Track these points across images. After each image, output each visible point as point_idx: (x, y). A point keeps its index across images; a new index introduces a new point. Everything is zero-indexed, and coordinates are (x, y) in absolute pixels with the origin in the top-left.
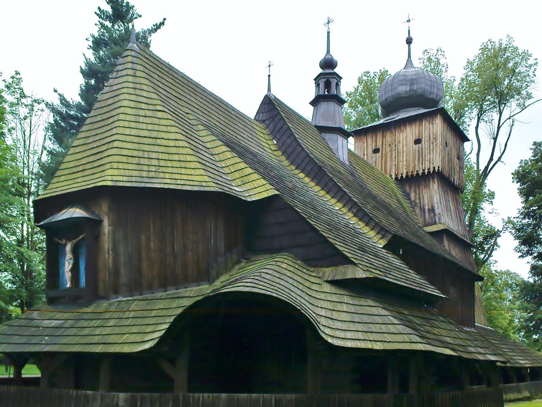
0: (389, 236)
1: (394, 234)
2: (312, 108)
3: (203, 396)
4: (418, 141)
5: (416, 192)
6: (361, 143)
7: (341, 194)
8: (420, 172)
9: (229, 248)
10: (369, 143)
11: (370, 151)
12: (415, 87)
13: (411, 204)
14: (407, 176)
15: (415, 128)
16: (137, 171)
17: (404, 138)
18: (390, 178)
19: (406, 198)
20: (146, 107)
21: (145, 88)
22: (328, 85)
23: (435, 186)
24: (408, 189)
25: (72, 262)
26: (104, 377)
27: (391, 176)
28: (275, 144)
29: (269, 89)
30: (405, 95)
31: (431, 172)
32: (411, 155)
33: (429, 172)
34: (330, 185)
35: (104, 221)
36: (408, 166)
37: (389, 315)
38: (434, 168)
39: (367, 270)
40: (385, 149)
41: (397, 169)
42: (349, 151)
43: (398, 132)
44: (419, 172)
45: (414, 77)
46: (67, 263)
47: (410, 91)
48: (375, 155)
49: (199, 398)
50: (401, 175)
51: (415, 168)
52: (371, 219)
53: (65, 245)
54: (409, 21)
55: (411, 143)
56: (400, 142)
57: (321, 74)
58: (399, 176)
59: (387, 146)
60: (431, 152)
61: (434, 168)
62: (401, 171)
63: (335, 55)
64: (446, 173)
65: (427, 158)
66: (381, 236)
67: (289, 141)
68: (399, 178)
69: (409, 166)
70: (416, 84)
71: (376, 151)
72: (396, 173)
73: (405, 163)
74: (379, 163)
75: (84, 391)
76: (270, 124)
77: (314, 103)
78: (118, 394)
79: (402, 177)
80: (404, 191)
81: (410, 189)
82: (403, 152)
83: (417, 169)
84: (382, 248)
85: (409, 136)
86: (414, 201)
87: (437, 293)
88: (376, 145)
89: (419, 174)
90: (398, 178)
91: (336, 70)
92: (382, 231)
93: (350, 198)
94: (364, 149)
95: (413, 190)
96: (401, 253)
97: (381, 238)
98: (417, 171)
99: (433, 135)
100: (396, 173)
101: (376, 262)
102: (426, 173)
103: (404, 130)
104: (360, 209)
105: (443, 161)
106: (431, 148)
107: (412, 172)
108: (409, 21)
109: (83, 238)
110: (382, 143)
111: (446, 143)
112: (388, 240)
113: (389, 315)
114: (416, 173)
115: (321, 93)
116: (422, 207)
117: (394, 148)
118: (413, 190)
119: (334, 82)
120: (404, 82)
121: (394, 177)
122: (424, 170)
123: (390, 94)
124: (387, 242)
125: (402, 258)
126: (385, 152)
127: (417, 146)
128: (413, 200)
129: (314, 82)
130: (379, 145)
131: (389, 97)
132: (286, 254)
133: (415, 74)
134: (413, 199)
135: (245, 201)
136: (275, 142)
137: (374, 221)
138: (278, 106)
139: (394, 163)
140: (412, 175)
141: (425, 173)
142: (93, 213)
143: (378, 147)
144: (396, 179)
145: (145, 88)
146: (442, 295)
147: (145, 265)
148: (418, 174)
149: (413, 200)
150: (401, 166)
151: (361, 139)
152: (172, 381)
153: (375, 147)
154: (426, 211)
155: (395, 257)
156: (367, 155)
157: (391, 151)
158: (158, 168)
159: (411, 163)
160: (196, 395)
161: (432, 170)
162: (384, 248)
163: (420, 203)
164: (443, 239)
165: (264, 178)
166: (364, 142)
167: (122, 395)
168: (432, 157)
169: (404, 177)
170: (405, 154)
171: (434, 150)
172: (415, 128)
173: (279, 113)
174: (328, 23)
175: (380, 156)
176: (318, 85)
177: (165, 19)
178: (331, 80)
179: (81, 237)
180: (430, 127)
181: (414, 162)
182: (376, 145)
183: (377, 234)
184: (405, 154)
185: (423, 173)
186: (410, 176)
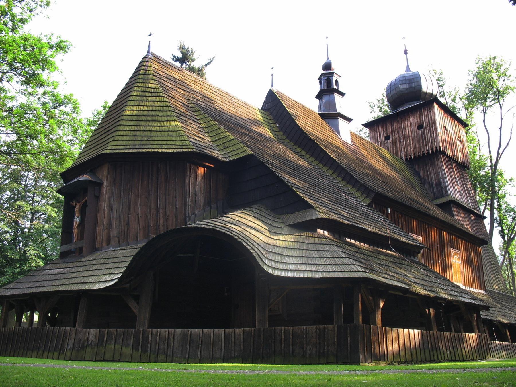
0: (373, 195)
2: (318, 101)
4: (420, 127)
5: (424, 170)
9: (208, 203)
11: (382, 138)
12: (413, 85)
13: (421, 180)
14: (415, 157)
15: (417, 116)
16: (132, 141)
17: (409, 125)
18: (401, 159)
28: (277, 127)
30: (406, 92)
31: (434, 151)
32: (416, 138)
33: (432, 152)
36: (414, 148)
37: (339, 251)
40: (395, 136)
41: (406, 152)
43: (403, 121)
44: (424, 153)
45: (412, 77)
47: (409, 88)
48: (386, 141)
49: (157, 334)
50: (409, 157)
51: (420, 150)
55: (415, 129)
56: (406, 129)
57: (322, 74)
59: (396, 133)
61: (436, 148)
65: (430, 140)
66: (366, 196)
68: (409, 159)
69: (416, 148)
70: (414, 82)
72: (405, 154)
73: (412, 145)
74: (390, 148)
76: (273, 111)
77: (319, 96)
79: (411, 158)
80: (414, 170)
82: (409, 137)
84: (366, 206)
85: (412, 124)
86: (423, 178)
88: (387, 133)
89: (424, 154)
90: (407, 159)
93: (339, 165)
94: (378, 137)
95: (421, 169)
97: (366, 197)
98: (423, 152)
100: (405, 154)
102: (430, 153)
103: (408, 118)
106: (432, 132)
107: (419, 153)
111: (445, 127)
112: (371, 199)
113: (339, 251)
114: (426, 152)
116: (430, 182)
117: (401, 134)
118: (421, 169)
120: (404, 82)
121: (404, 158)
122: (428, 150)
123: (394, 92)
124: (371, 200)
126: (395, 138)
127: (420, 131)
128: (422, 177)
129: (318, 81)
130: (389, 133)
131: (394, 94)
132: (258, 205)
133: (412, 75)
136: (278, 125)
138: (279, 96)
139: (403, 146)
140: (419, 155)
141: (429, 153)
143: (388, 135)
144: (406, 159)
148: (423, 154)
149: (422, 176)
150: (409, 148)
151: (374, 129)
153: (386, 135)
154: (434, 186)
156: (380, 141)
157: (399, 137)
158: (149, 137)
159: (417, 145)
166: (377, 132)
168: (433, 139)
170: (411, 138)
171: (434, 133)
172: (417, 116)
175: (391, 141)
176: (321, 83)
180: (428, 114)
181: (419, 144)
183: (362, 194)
184: (411, 138)
186: (417, 157)
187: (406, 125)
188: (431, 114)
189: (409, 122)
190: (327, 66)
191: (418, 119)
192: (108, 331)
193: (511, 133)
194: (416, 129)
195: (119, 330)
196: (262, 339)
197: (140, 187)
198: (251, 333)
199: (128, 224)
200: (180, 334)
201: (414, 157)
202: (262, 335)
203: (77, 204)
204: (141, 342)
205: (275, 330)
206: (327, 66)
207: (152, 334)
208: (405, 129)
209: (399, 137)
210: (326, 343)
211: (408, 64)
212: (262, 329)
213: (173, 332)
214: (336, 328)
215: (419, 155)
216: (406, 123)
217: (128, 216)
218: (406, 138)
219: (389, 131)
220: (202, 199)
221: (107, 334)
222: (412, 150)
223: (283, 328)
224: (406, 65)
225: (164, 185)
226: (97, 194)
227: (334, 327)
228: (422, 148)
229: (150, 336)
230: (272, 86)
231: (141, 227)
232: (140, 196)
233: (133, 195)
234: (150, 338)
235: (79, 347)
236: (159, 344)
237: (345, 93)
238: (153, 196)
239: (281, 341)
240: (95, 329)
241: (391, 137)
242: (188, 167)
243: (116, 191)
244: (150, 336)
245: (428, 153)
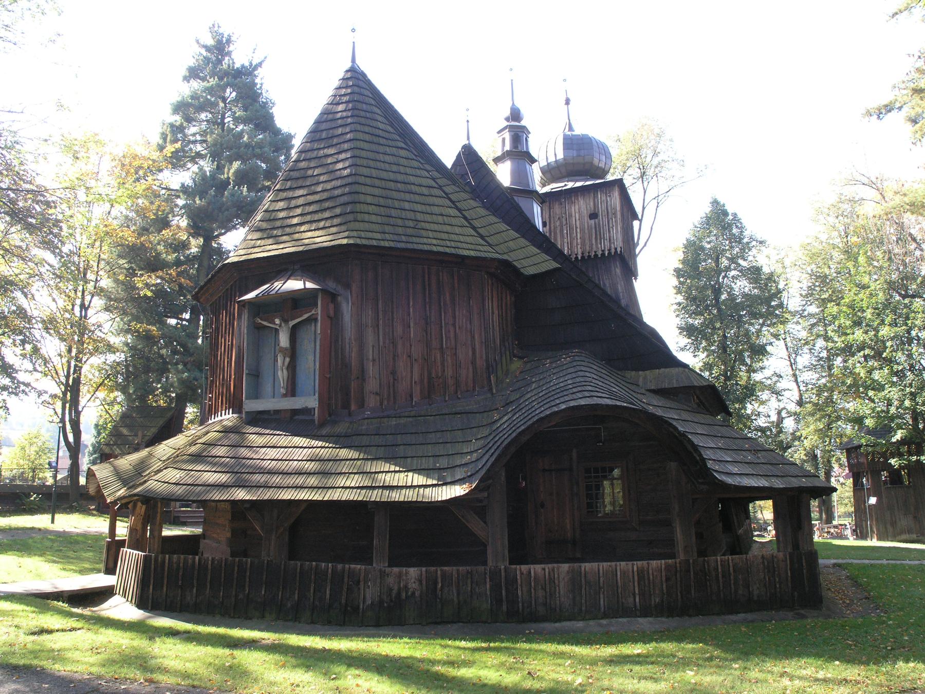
4: (593, 216)
8: (599, 253)
12: (582, 153)
14: (583, 257)
17: (577, 211)
33: (610, 253)
54: (468, 110)
60: (611, 229)
61: (616, 249)
63: (518, 105)
73: (579, 241)
75: (347, 566)
78: (648, 563)
82: (576, 228)
99: (612, 210)
106: (611, 225)
110: (550, 215)
114: (600, 252)
127: (592, 222)
140: (589, 256)
148: (596, 255)
157: (561, 226)
159: (587, 241)
161: (613, 251)
167: (413, 572)
169: (579, 258)
170: (578, 230)
177: (265, 58)
178: (520, 134)
184: (578, 230)
187: (573, 210)
188: (611, 201)
189: (577, 207)
190: (515, 115)
191: (592, 204)
192: (442, 570)
193: (652, 228)
194: (586, 218)
195: (461, 568)
198: (676, 567)
200: (568, 572)
201: (582, 257)
204: (504, 588)
206: (515, 115)
207: (522, 574)
208: (570, 216)
209: (561, 226)
210: (777, 579)
212: (691, 561)
215: (589, 256)
216: (573, 208)
218: (571, 228)
221: (442, 576)
222: (579, 247)
228: (594, 246)
230: (468, 139)
231: (416, 380)
235: (391, 601)
236: (535, 589)
237: (707, 209)
239: (717, 576)
240: (416, 569)
241: (548, 224)
243: (370, 312)
245: (603, 254)
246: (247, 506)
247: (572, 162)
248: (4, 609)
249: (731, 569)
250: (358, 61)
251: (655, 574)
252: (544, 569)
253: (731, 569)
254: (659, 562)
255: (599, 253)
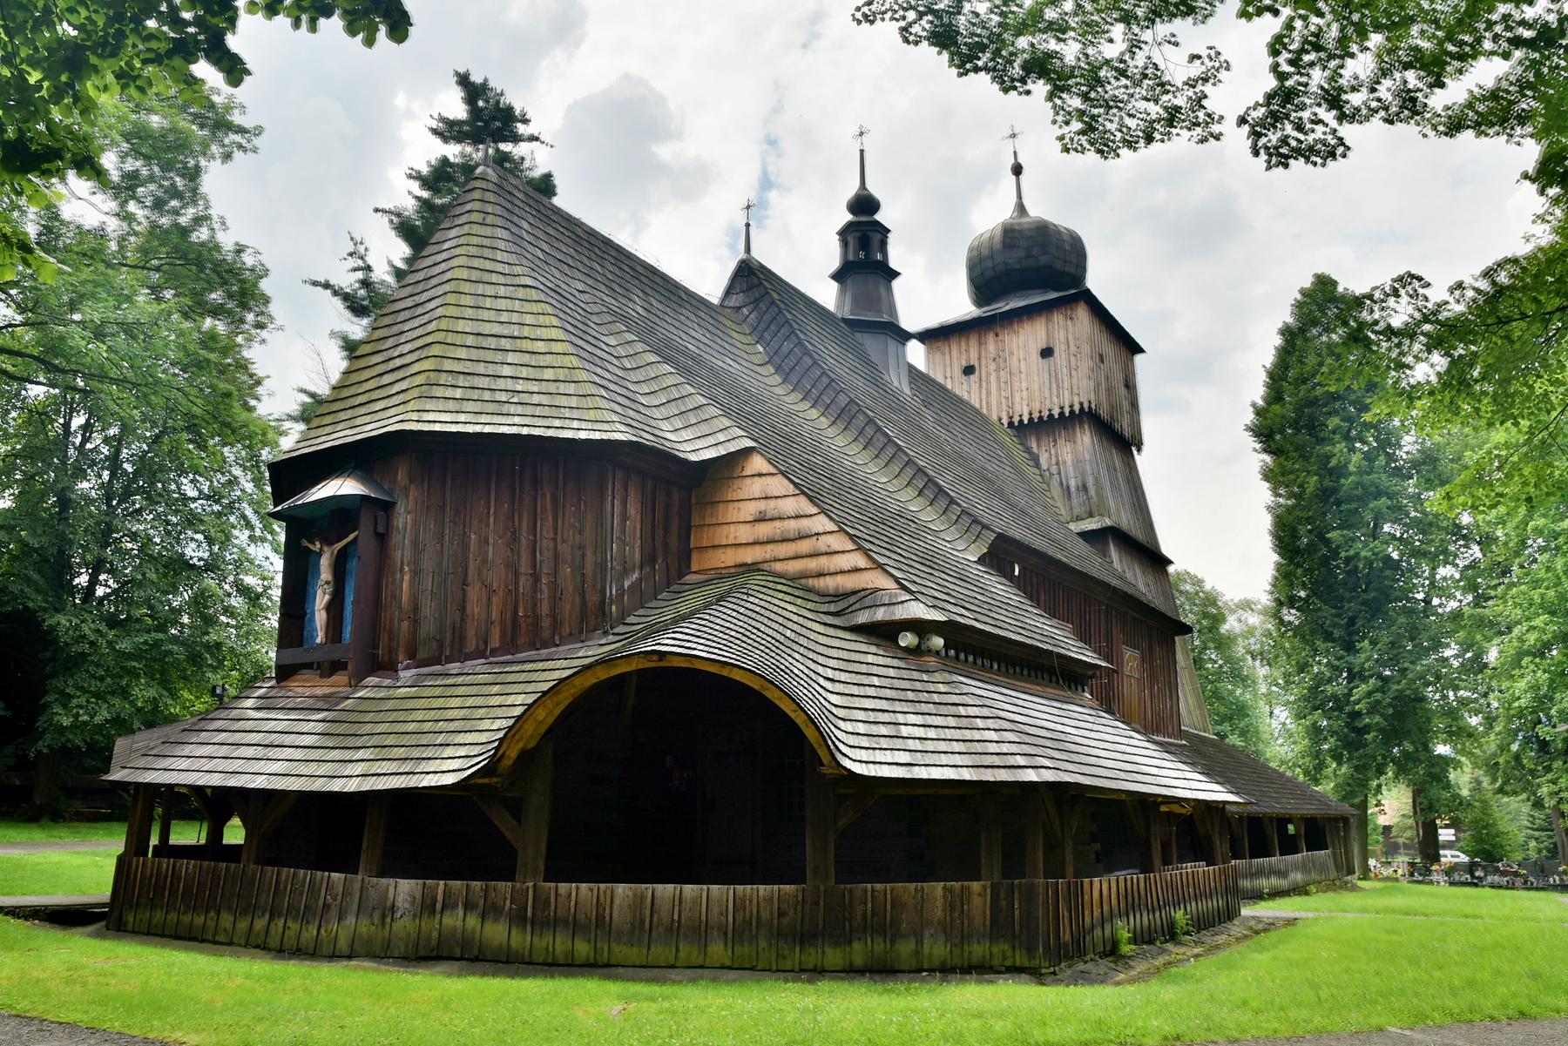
1: (999, 534)
2: (835, 285)
3: (578, 888)
4: (1047, 353)
6: (938, 356)
7: (890, 451)
8: (1056, 413)
10: (960, 353)
14: (1031, 419)
19: (1031, 463)
20: (502, 280)
21: (502, 245)
22: (864, 243)
23: (1085, 439)
24: (1034, 445)
25: (329, 589)
26: (370, 848)
27: (1000, 419)
29: (748, 249)
33: (1072, 412)
34: (869, 431)
35: (398, 506)
36: (1030, 400)
38: (1081, 404)
39: (934, 607)
42: (912, 370)
46: (319, 592)
49: (570, 895)
52: (952, 501)
53: (320, 555)
54: (1013, 136)
58: (1016, 420)
61: (1081, 404)
62: (1017, 409)
63: (874, 189)
64: (1104, 413)
67: (787, 346)
71: (969, 370)
80: (1028, 450)
81: (1039, 446)
83: (1048, 405)
87: (1089, 657)
88: (968, 359)
91: (878, 217)
92: (974, 524)
96: (1017, 573)
101: (960, 590)
104: (930, 480)
105: (1097, 391)
108: (1013, 136)
109: (355, 539)
115: (851, 258)
119: (876, 237)
121: (1005, 421)
122: (1062, 408)
125: (1022, 585)
134: (1044, 466)
135: (686, 461)
136: (761, 349)
137: (959, 505)
139: (1003, 394)
140: (1041, 418)
142: (385, 492)
144: (1011, 424)
145: (502, 245)
146: (1099, 663)
147: (474, 593)
148: (1051, 416)
152: (512, 853)
155: (1005, 581)
160: (563, 887)
162: (981, 561)
163: (1059, 473)
164: (1109, 549)
165: (727, 415)
173: (767, 293)
174: (861, 134)
178: (871, 234)
179: (352, 536)
182: (968, 359)
185: (1062, 414)
190: (864, 205)
196: (821, 912)
197: (492, 519)
199: (463, 609)
202: (822, 904)
203: (325, 548)
205: (851, 892)
206: (864, 205)
207: (557, 895)
211: (1019, 196)
213: (609, 892)
214: (988, 891)
217: (464, 590)
219: (974, 354)
220: (637, 550)
223: (869, 886)
224: (1014, 199)
225: (550, 518)
226: (381, 530)
227: (984, 887)
229: (552, 900)
232: (491, 541)
233: (473, 536)
234: (553, 905)
238: (524, 542)
242: (610, 474)
244: (552, 900)
246: (1160, 799)
247: (1017, 266)
248: (1331, 895)
249: (889, 904)
250: (868, 186)
251: (762, 905)
252: (591, 890)
253: (889, 904)
254: (769, 887)
255: (1056, 413)
